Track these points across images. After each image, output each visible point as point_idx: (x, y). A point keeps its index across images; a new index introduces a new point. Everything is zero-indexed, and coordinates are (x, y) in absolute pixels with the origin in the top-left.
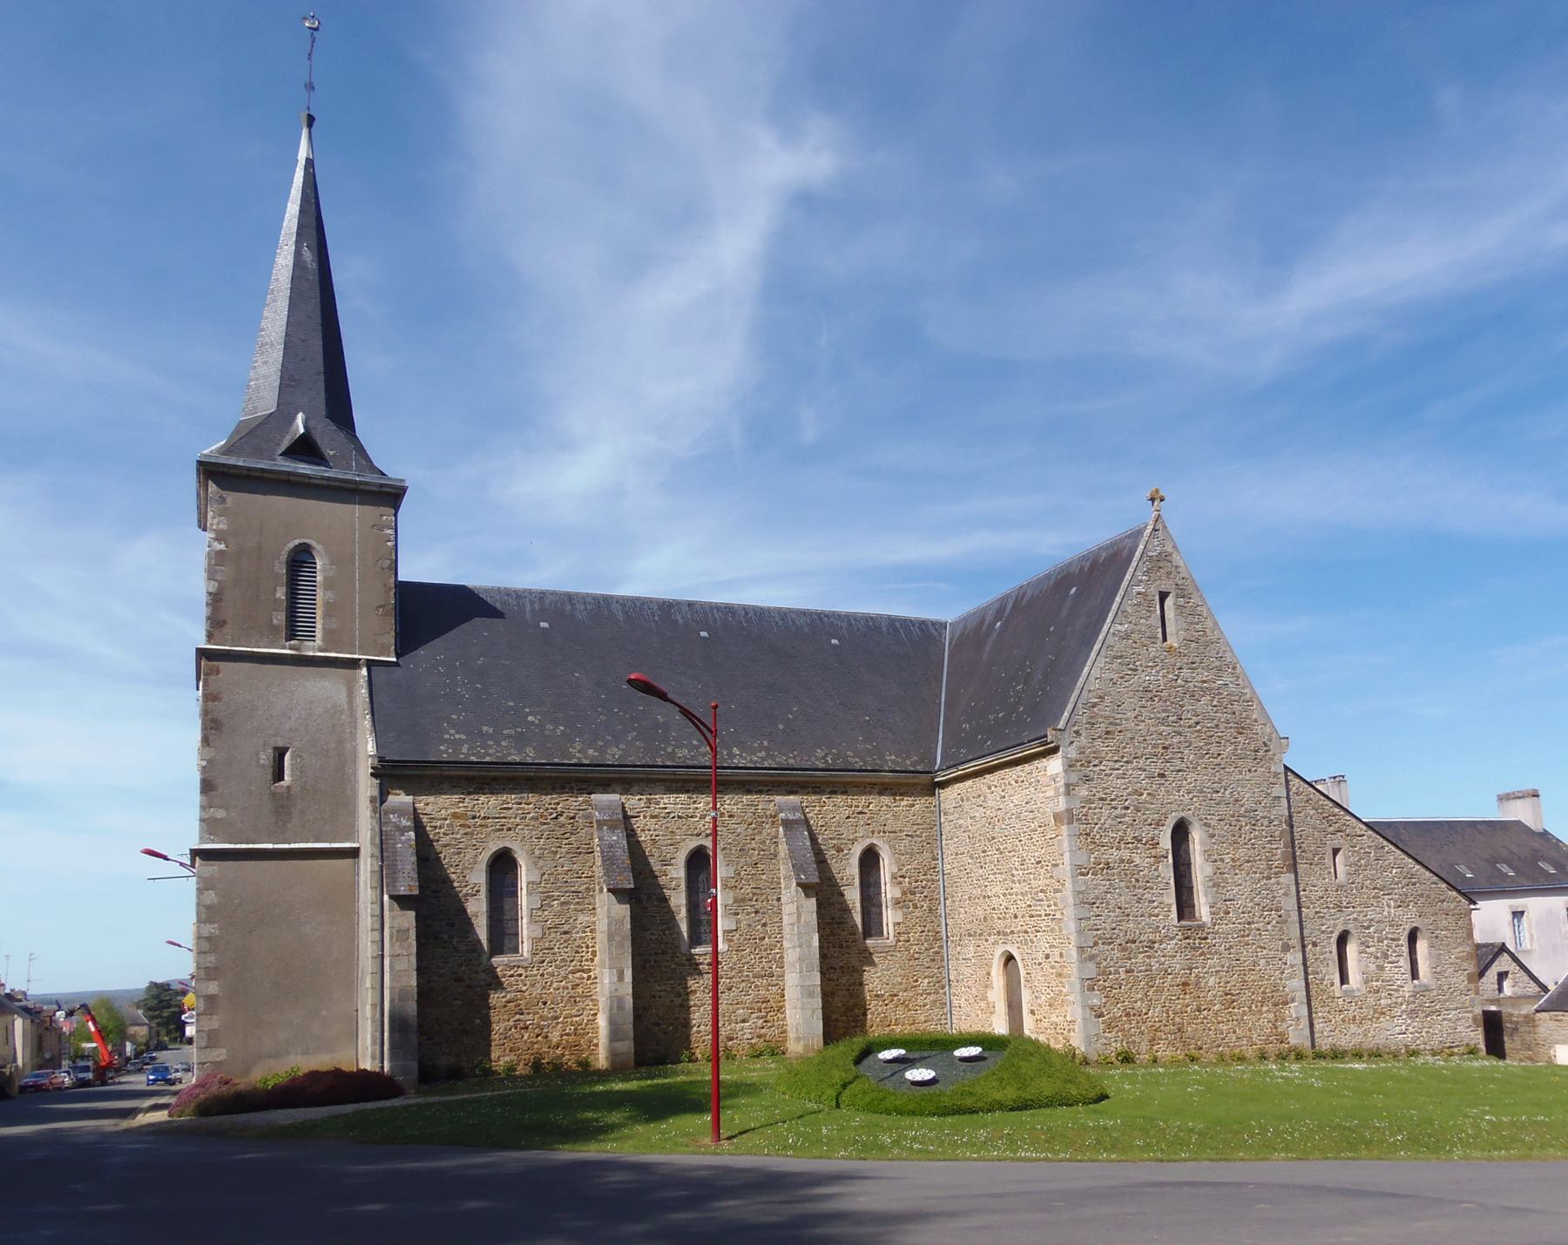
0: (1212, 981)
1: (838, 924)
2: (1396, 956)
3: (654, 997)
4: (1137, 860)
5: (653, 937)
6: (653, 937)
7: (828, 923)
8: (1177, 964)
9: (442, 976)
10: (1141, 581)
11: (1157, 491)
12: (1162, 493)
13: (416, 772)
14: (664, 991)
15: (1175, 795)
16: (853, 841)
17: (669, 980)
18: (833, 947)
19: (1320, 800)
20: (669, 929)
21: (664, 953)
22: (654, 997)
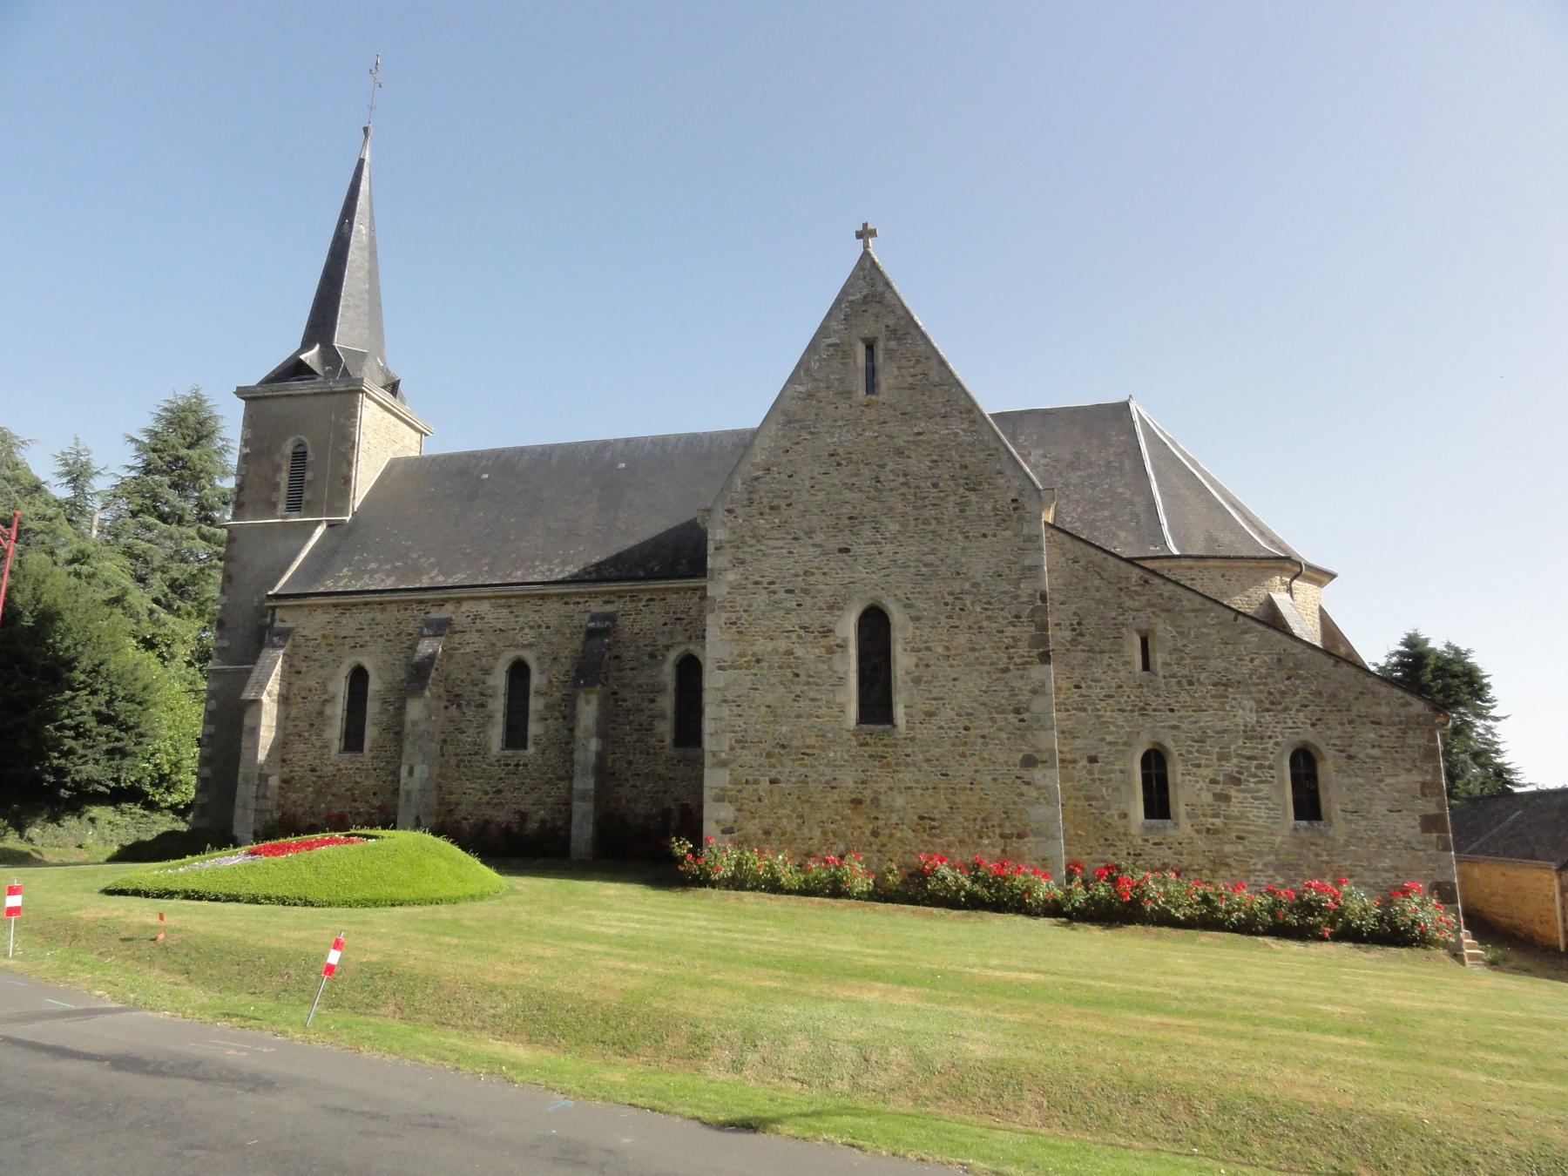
0: (900, 801)
1: (646, 730)
2: (1255, 783)
3: (465, 793)
4: (799, 652)
5: (469, 739)
6: (469, 739)
7: (636, 730)
8: (848, 779)
9: (302, 766)
10: (835, 331)
11: (865, 225)
12: (870, 227)
13: (296, 602)
14: (473, 789)
15: (861, 572)
16: (667, 648)
17: (479, 778)
18: (640, 753)
19: (491, 573)
20: (483, 732)
21: (476, 754)
22: (465, 793)
